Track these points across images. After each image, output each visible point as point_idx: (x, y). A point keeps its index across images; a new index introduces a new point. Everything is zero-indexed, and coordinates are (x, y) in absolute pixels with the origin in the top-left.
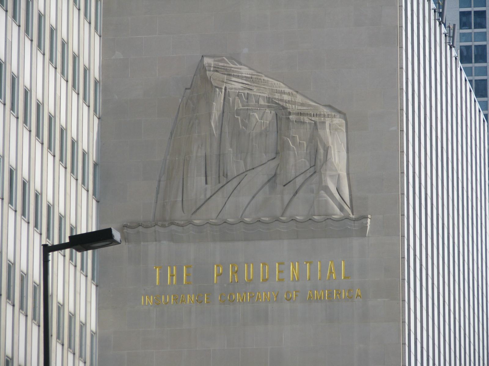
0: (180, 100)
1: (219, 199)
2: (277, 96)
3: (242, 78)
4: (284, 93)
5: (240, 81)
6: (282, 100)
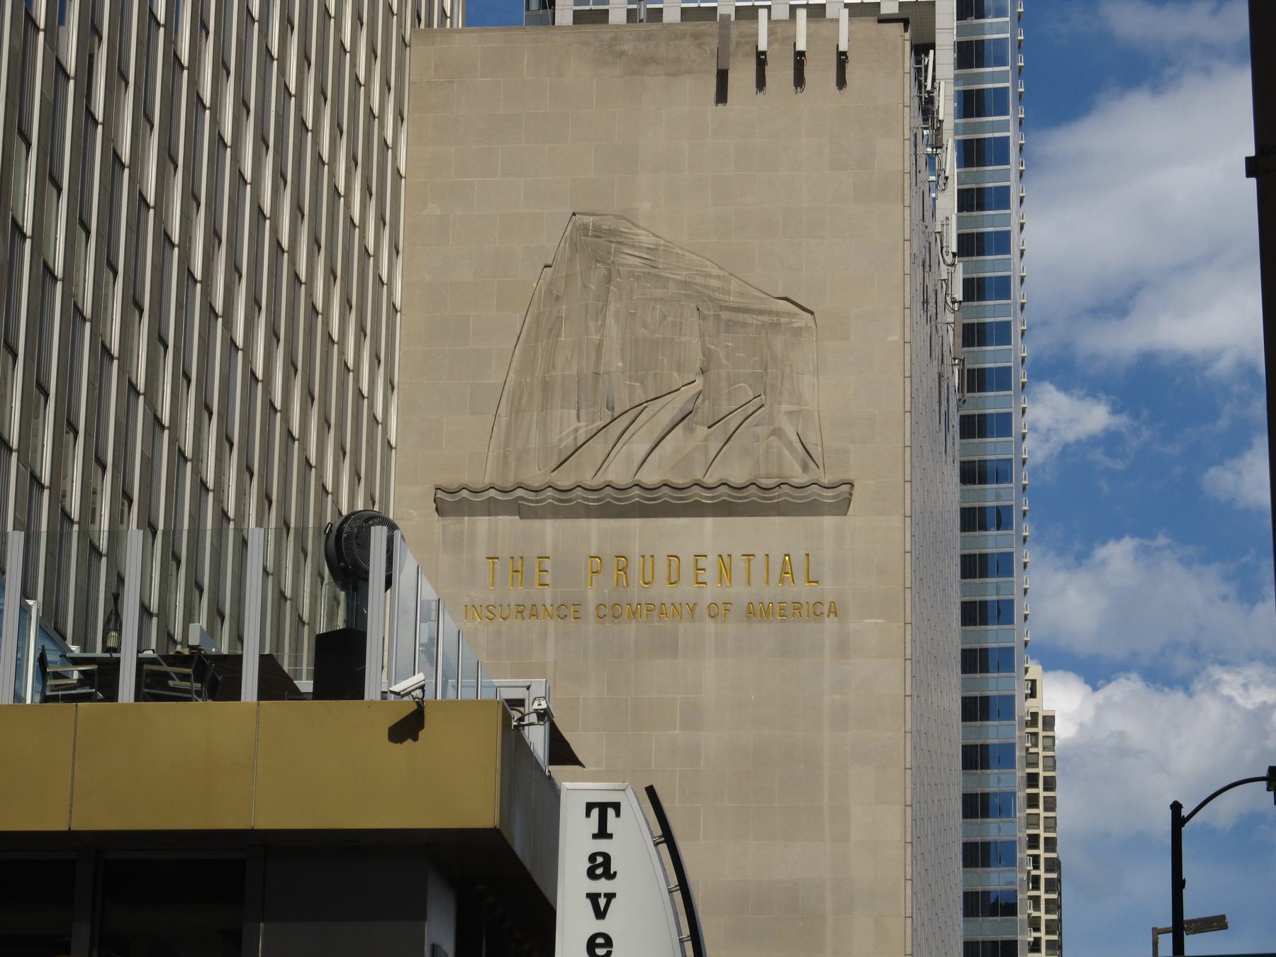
1: (599, 446)
2: (699, 280)
4: (710, 276)
5: (637, 254)
6: (706, 286)
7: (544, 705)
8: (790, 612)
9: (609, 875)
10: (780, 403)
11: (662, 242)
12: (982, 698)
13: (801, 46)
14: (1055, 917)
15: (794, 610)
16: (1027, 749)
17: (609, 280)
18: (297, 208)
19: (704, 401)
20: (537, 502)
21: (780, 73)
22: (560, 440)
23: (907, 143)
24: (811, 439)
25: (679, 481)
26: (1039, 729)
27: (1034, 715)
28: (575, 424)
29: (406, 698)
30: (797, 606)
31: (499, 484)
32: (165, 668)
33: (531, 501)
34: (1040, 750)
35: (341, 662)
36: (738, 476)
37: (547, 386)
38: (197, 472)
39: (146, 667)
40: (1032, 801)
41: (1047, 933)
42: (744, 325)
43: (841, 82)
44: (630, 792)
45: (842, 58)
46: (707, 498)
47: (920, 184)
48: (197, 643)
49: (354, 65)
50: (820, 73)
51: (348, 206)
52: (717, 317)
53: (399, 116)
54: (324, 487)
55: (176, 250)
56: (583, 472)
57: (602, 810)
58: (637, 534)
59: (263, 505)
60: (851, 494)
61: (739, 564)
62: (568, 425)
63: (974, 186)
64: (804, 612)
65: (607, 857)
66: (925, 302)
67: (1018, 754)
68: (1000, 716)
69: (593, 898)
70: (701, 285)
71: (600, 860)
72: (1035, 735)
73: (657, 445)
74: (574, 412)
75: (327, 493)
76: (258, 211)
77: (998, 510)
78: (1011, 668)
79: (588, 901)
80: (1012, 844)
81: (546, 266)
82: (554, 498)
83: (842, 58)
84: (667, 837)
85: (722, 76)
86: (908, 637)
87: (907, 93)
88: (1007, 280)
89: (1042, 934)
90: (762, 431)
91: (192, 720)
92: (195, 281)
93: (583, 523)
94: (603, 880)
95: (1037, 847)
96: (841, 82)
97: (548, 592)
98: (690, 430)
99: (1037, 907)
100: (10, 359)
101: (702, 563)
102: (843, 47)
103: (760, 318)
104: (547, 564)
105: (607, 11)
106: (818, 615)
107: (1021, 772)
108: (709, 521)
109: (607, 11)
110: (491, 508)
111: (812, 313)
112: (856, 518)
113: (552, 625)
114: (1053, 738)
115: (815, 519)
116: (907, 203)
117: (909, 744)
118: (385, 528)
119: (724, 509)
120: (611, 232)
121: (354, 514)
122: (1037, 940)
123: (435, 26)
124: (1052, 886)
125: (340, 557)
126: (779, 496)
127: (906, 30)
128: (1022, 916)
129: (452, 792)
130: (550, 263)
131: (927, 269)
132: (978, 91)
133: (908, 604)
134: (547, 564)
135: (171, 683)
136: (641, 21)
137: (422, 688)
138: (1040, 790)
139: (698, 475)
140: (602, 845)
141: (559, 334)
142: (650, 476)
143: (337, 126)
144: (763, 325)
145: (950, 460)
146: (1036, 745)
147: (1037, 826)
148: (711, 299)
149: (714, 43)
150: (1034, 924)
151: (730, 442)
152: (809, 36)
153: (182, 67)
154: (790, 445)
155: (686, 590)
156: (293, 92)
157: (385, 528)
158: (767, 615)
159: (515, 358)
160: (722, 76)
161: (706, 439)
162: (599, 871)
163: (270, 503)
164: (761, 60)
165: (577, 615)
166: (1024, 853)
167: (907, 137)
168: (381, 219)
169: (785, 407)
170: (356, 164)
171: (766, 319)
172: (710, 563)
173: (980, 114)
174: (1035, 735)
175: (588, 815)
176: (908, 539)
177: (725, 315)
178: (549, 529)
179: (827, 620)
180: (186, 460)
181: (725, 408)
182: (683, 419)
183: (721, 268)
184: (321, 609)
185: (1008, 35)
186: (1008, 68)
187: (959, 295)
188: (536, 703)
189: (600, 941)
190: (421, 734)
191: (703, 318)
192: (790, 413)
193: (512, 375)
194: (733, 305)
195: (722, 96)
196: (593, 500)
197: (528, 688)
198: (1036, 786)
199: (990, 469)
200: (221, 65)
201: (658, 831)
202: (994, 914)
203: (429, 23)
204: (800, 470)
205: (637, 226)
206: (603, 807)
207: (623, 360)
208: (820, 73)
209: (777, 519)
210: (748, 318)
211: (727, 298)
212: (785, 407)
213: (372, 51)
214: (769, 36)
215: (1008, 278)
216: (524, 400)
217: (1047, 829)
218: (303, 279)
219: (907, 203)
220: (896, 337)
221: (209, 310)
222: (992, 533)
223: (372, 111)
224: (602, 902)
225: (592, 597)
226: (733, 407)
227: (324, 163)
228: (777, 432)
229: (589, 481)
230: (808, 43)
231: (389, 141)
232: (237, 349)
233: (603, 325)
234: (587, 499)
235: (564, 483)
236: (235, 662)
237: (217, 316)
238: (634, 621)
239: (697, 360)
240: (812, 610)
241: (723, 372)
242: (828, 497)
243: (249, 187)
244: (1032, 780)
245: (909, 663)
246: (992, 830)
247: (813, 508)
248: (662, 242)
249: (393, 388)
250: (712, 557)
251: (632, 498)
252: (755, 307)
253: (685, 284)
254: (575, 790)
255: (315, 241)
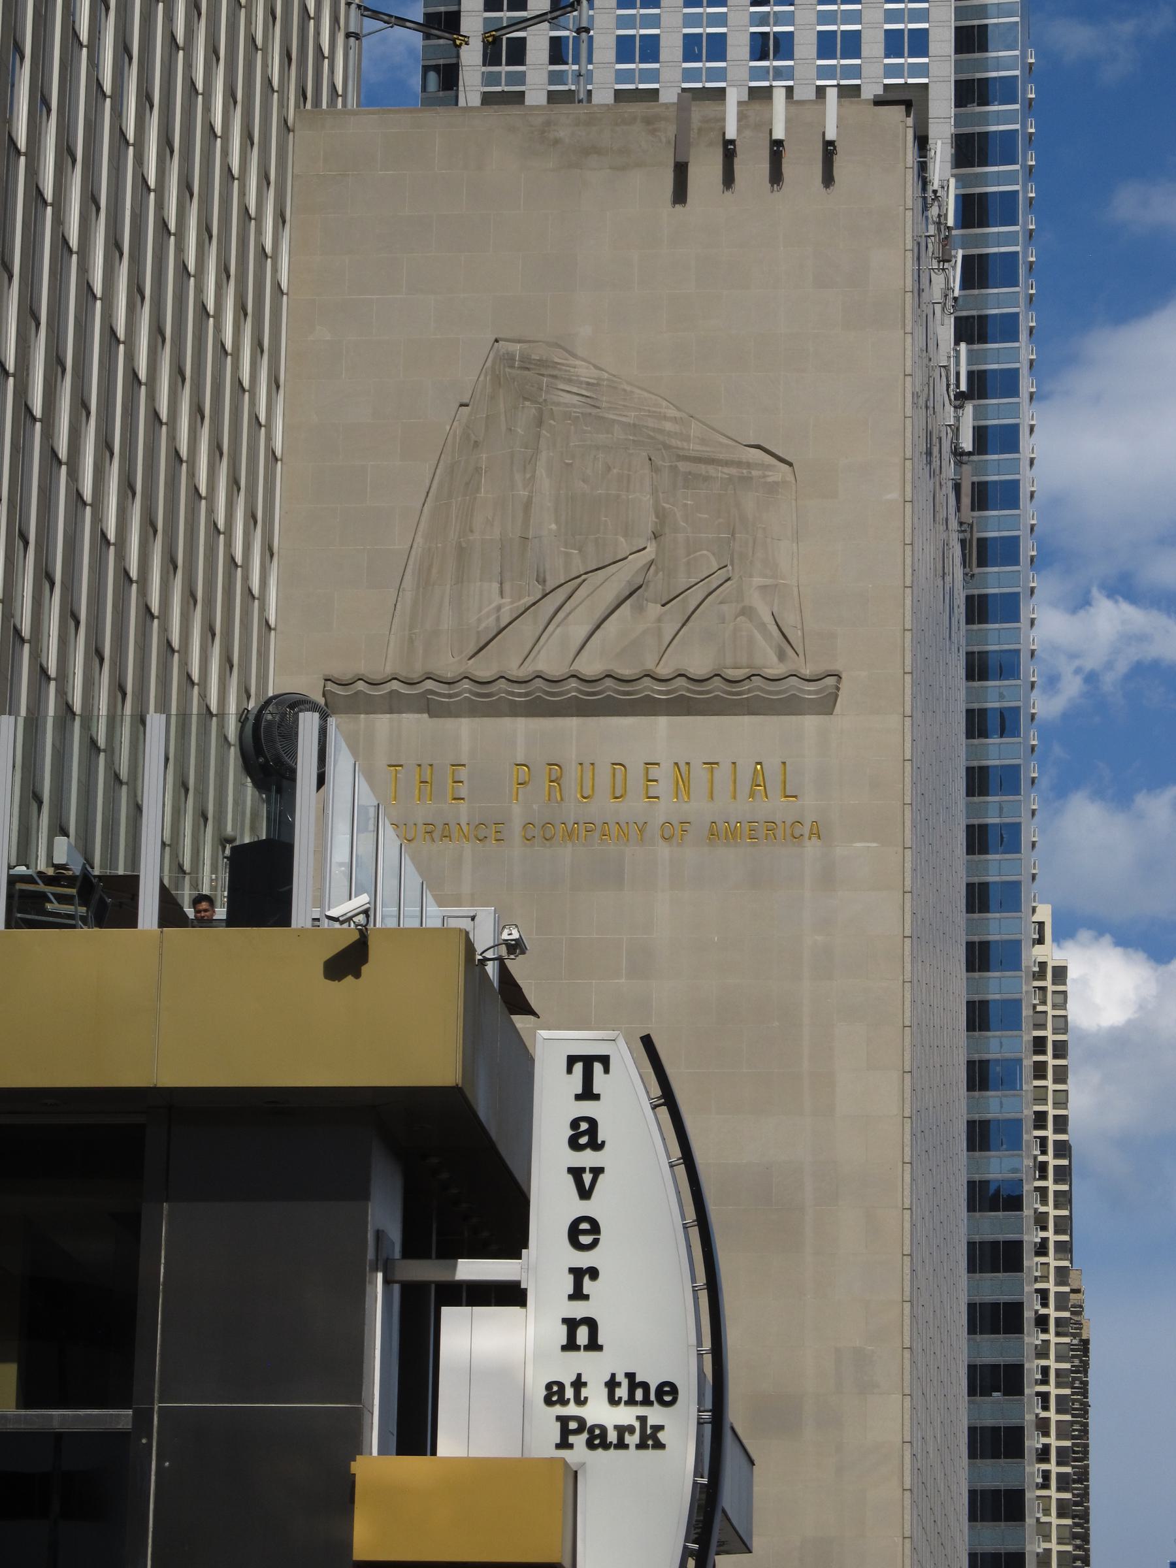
0: (448, 428)
1: (527, 628)
2: (651, 423)
3: (579, 383)
4: (665, 418)
5: (575, 390)
6: (661, 431)
7: (516, 935)
8: (762, 835)
9: (596, 1145)
10: (751, 576)
11: (606, 375)
12: (981, 943)
13: (779, 133)
14: (1066, 1213)
15: (764, 832)
16: (1035, 1006)
17: (540, 423)
18: (158, 331)
19: (656, 572)
20: (450, 696)
21: (752, 167)
22: (479, 620)
23: (909, 254)
24: (790, 620)
25: (626, 672)
26: (1048, 983)
27: (1043, 965)
28: (498, 600)
29: (345, 926)
30: (771, 826)
31: (403, 673)
32: (41, 887)
33: (444, 696)
34: (1048, 1008)
35: (261, 884)
36: (699, 666)
37: (462, 553)
38: (36, 655)
39: (19, 886)
40: (1040, 1071)
41: (1056, 1232)
42: (706, 479)
43: (828, 179)
44: (621, 1042)
45: (829, 149)
46: (660, 692)
47: (923, 306)
48: (64, 862)
49: (225, 153)
50: (802, 167)
51: (218, 329)
52: (674, 469)
53: (281, 218)
54: (189, 677)
55: (11, 380)
56: (507, 660)
57: (587, 1065)
58: (572, 733)
59: (115, 697)
60: (838, 689)
61: (699, 774)
62: (488, 602)
63: (974, 313)
64: (780, 832)
65: (593, 1122)
66: (929, 453)
67: (1024, 1013)
68: (1002, 966)
69: (576, 1173)
70: (654, 430)
71: (584, 1126)
72: (1043, 989)
73: (598, 627)
74: (496, 586)
75: (193, 683)
76: (110, 333)
77: (1002, 713)
78: (1017, 908)
79: (570, 1178)
80: (1019, 1122)
81: (462, 405)
82: (470, 692)
83: (829, 149)
84: (668, 1099)
85: (681, 171)
86: (908, 865)
87: (909, 192)
88: (1015, 428)
89: (1050, 1234)
90: (728, 609)
91: (78, 952)
92: (34, 419)
93: (507, 722)
94: (588, 1151)
95: (1044, 1127)
96: (828, 179)
97: (463, 806)
98: (640, 609)
99: (1044, 1202)
100: (108, 454)
101: (654, 772)
102: (831, 135)
103: (726, 470)
104: (463, 773)
105: (523, 93)
106: (797, 838)
107: (1029, 1034)
108: (663, 721)
109: (523, 93)
110: (393, 704)
111: (790, 464)
112: (844, 718)
113: (468, 848)
114: (1065, 993)
115: (794, 718)
116: (909, 329)
117: (908, 996)
118: (316, 715)
119: (681, 706)
120: (543, 363)
121: (268, 702)
122: (1045, 1241)
123: (324, 106)
124: (1063, 1174)
125: (259, 751)
126: (749, 691)
127: (908, 115)
128: (1027, 1212)
129: (406, 1043)
130: (466, 401)
131: (931, 411)
132: (980, 195)
133: (908, 824)
134: (463, 773)
135: (49, 906)
136: (580, 101)
137: (366, 912)
138: (1048, 1058)
139: (650, 665)
140: (587, 1108)
141: (478, 490)
142: (590, 666)
143: (205, 229)
144: (731, 478)
145: (954, 648)
146: (1044, 1003)
147: (1044, 1101)
148: (667, 447)
149: (671, 130)
150: (1041, 1221)
151: (689, 624)
152: (788, 121)
153: (18, 153)
154: (762, 627)
155: (634, 806)
156: (152, 186)
157: (316, 715)
158: (734, 838)
159: (423, 519)
160: (681, 171)
161: (659, 620)
162: (584, 1140)
163: (124, 695)
164: (729, 150)
165: (499, 836)
166: (1031, 1134)
167: (909, 247)
168: (258, 345)
169: (757, 581)
170: (228, 277)
171: (733, 471)
172: (664, 774)
173: (983, 223)
174: (1043, 989)
175: (569, 1071)
176: (908, 745)
177: (683, 466)
178: (465, 728)
179: (807, 843)
180: (23, 641)
181: (682, 581)
182: (631, 595)
183: (678, 409)
184: (242, 812)
185: (1017, 127)
186: (1017, 167)
187: (967, 444)
188: (506, 931)
189: (584, 1226)
190: (364, 969)
191: (655, 469)
192: (763, 588)
193: (419, 540)
194: (693, 454)
195: (680, 195)
196: (520, 695)
197: (473, 918)
198: (1044, 1053)
199: (992, 662)
200: (66, 151)
201: (656, 1091)
202: (994, 1208)
203: (317, 102)
204: (775, 659)
205: (574, 356)
206: (588, 1061)
207: (557, 522)
208: (802, 167)
209: (747, 719)
210: (711, 470)
211: (685, 445)
212: (757, 581)
213: (248, 136)
214: (739, 120)
215: (1017, 426)
216: (434, 571)
217: (1056, 1105)
218: (164, 418)
219: (909, 329)
220: (894, 495)
221: (51, 455)
222: (994, 740)
223: (247, 210)
224: (587, 1178)
225: (517, 813)
226: (693, 580)
227: (189, 275)
228: (747, 612)
229: (515, 672)
230: (787, 129)
231: (269, 249)
232: (85, 504)
233: (533, 477)
234: (513, 694)
235: (484, 673)
236: (130, 885)
237: (60, 463)
238: (569, 844)
239: (648, 522)
240: (789, 831)
241: (681, 537)
242: (810, 693)
243: (99, 303)
244: (1039, 1045)
245: (908, 896)
246: (995, 1105)
247: (791, 706)
248: (606, 375)
249: (272, 555)
250: (666, 766)
251: (568, 691)
252: (721, 456)
253: (635, 427)
254: (551, 1045)
255: (178, 372)
